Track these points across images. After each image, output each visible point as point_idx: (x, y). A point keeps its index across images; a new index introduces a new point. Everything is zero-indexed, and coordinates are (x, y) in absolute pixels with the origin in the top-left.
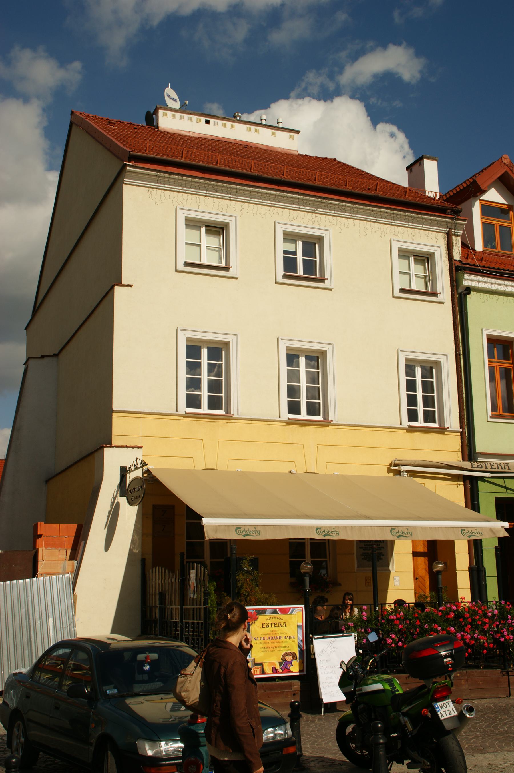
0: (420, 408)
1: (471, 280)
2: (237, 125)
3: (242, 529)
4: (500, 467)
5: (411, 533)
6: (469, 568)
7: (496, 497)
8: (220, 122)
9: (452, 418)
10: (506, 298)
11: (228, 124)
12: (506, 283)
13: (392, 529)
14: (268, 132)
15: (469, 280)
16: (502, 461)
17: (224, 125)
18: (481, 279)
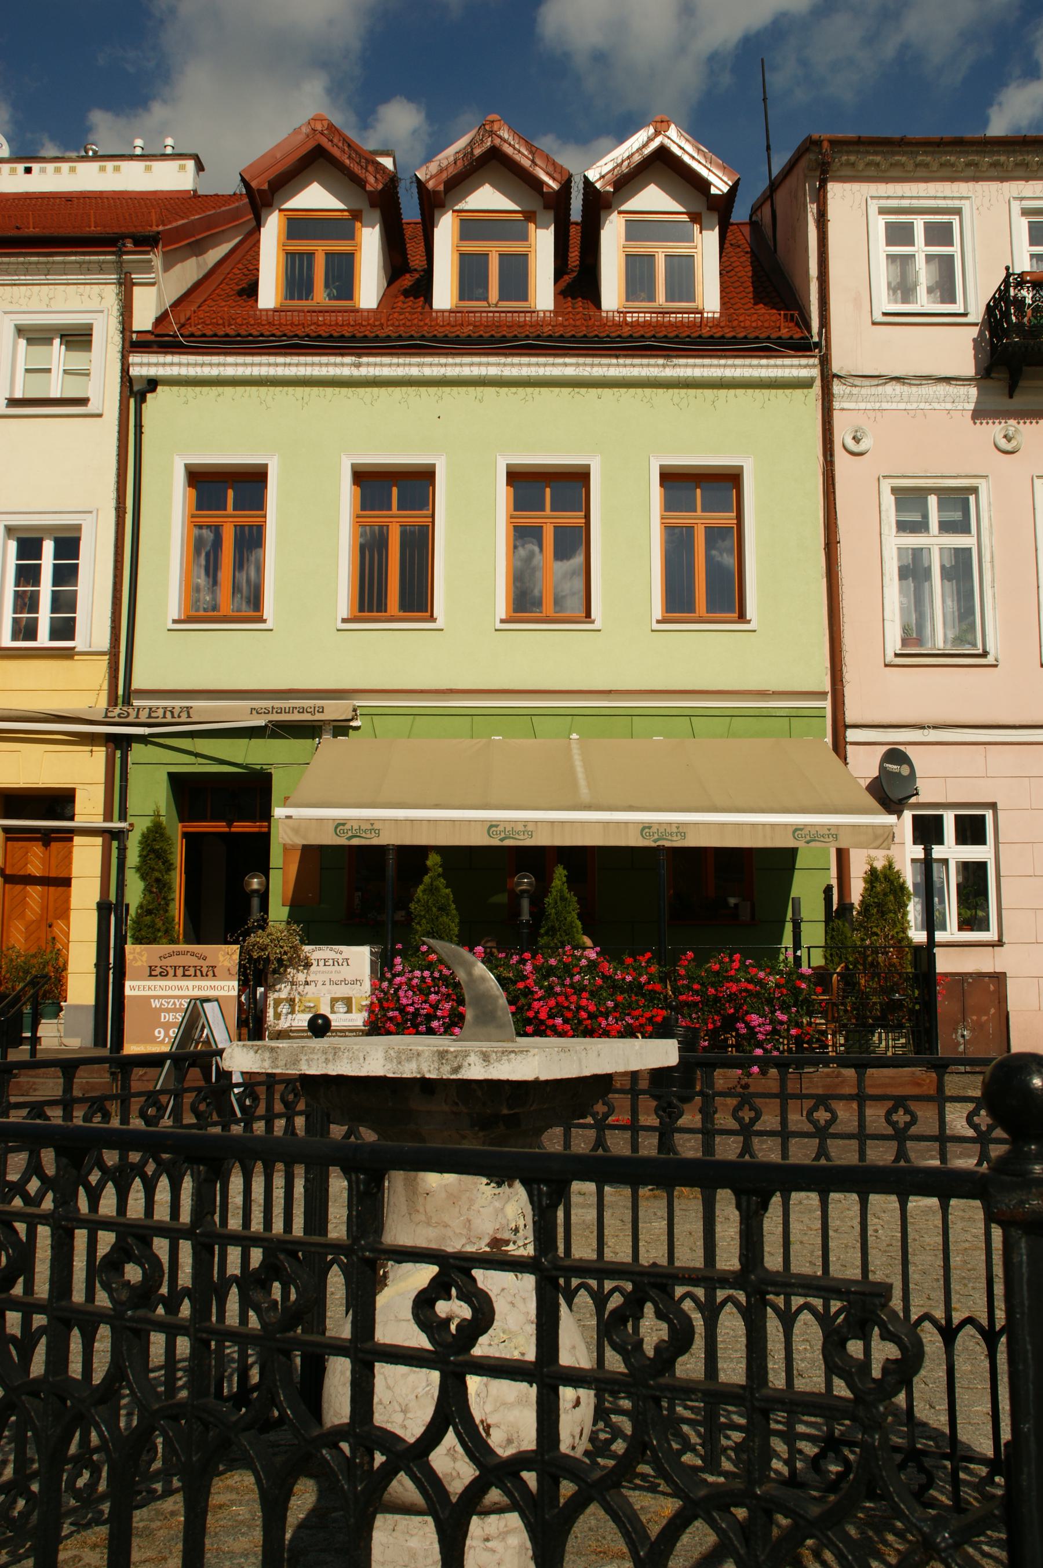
0: (44, 616)
1: (149, 364)
2: (81, 166)
3: (501, 828)
4: (168, 714)
5: (836, 837)
6: (98, 904)
7: (169, 774)
8: (50, 167)
9: (93, 625)
10: (240, 390)
11: (65, 166)
12: (257, 359)
13: (797, 829)
14: (138, 166)
15: (144, 365)
16: (178, 704)
17: (58, 170)
18: (184, 359)
